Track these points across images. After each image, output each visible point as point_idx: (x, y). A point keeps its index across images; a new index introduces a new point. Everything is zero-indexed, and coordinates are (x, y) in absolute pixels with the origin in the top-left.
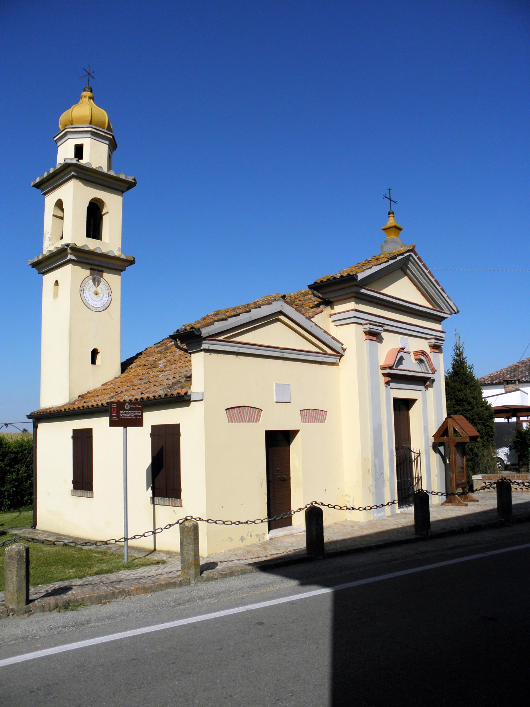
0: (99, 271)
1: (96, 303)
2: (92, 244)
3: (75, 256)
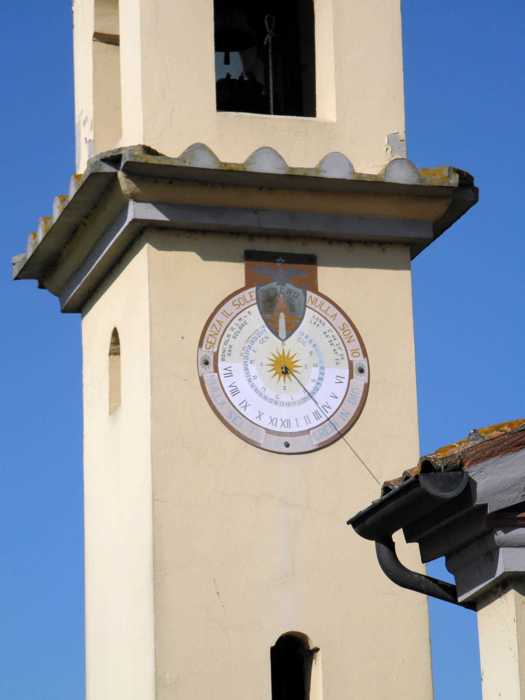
0: (292, 259)
1: (284, 413)
2: (245, 140)
3: (157, 204)
